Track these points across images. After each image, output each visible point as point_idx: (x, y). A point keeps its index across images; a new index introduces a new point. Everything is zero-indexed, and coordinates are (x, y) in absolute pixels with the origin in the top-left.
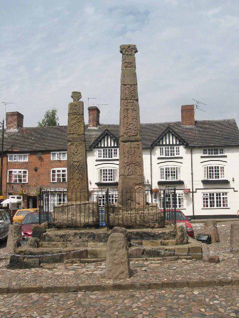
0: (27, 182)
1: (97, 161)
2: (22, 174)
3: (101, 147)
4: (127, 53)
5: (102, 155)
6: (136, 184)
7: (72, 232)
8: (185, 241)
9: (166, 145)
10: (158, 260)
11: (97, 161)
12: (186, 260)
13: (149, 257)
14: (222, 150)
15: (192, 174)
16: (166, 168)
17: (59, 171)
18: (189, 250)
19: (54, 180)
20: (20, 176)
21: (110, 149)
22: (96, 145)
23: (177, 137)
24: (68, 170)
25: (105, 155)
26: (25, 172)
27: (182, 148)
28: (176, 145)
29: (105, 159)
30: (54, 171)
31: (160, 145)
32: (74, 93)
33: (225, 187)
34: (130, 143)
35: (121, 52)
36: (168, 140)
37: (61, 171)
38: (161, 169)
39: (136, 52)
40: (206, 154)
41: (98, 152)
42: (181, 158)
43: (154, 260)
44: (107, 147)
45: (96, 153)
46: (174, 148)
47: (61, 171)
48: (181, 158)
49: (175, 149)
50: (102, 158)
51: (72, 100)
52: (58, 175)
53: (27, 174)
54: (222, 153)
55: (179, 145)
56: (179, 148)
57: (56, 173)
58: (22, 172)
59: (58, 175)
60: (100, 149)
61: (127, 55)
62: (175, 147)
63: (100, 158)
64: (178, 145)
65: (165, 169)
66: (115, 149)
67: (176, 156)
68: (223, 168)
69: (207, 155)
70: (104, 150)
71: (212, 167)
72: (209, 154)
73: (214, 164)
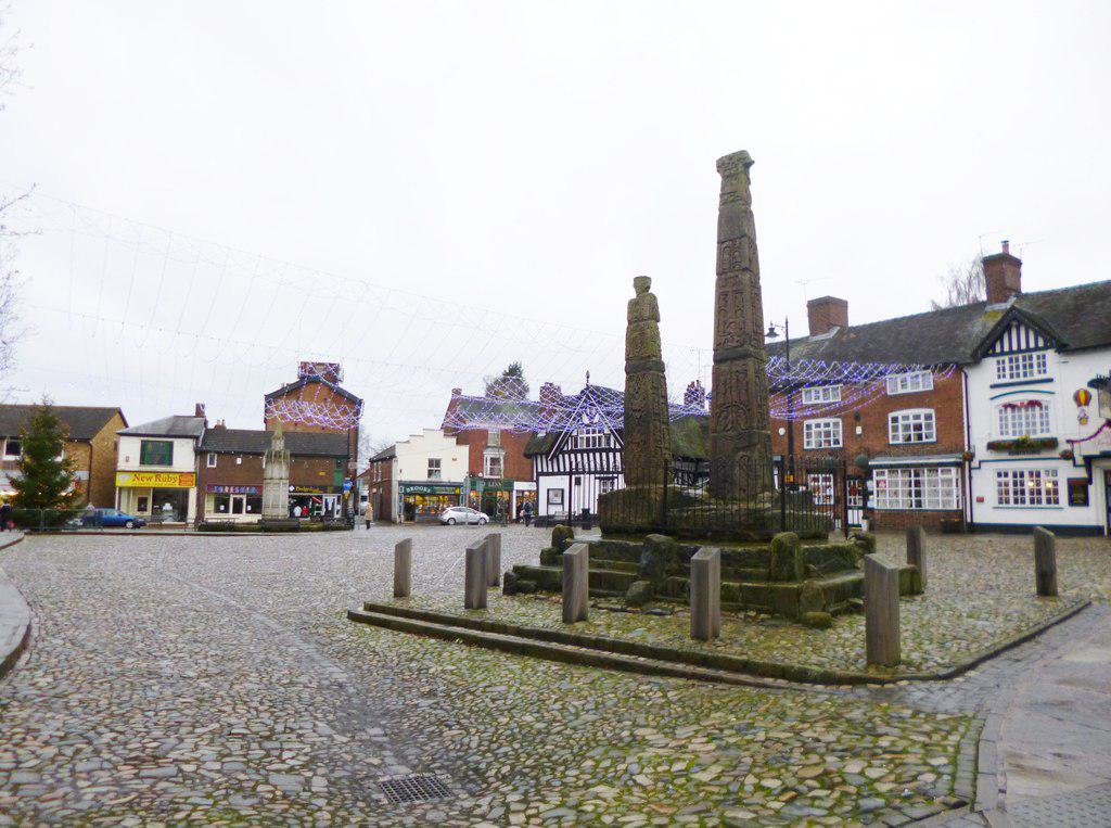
0: (841, 445)
1: (993, 387)
2: (922, 421)
3: (1003, 353)
5: (1008, 372)
6: (739, 449)
7: (1075, 609)
9: (1011, 352)
11: (993, 387)
17: (818, 426)
19: (808, 443)
20: (918, 427)
21: (1027, 354)
22: (986, 348)
23: (1041, 331)
24: (937, 412)
25: (1015, 372)
26: (836, 424)
27: (1051, 355)
28: (1037, 348)
29: (1016, 380)
30: (809, 427)
31: (995, 355)
32: (636, 279)
33: (1049, 456)
34: (728, 363)
36: (550, 466)
37: (911, 417)
41: (995, 367)
42: (1051, 380)
44: (594, 451)
45: (990, 364)
46: (1031, 358)
47: (911, 417)
48: (1051, 380)
49: (1035, 361)
50: (1007, 380)
52: (907, 427)
53: (934, 421)
55: (1046, 348)
56: (1044, 357)
57: (901, 422)
58: (923, 418)
59: (907, 427)
60: (1001, 358)
62: (1035, 355)
63: (1002, 381)
64: (1040, 349)
66: (1041, 353)
67: (1037, 377)
70: (1011, 360)
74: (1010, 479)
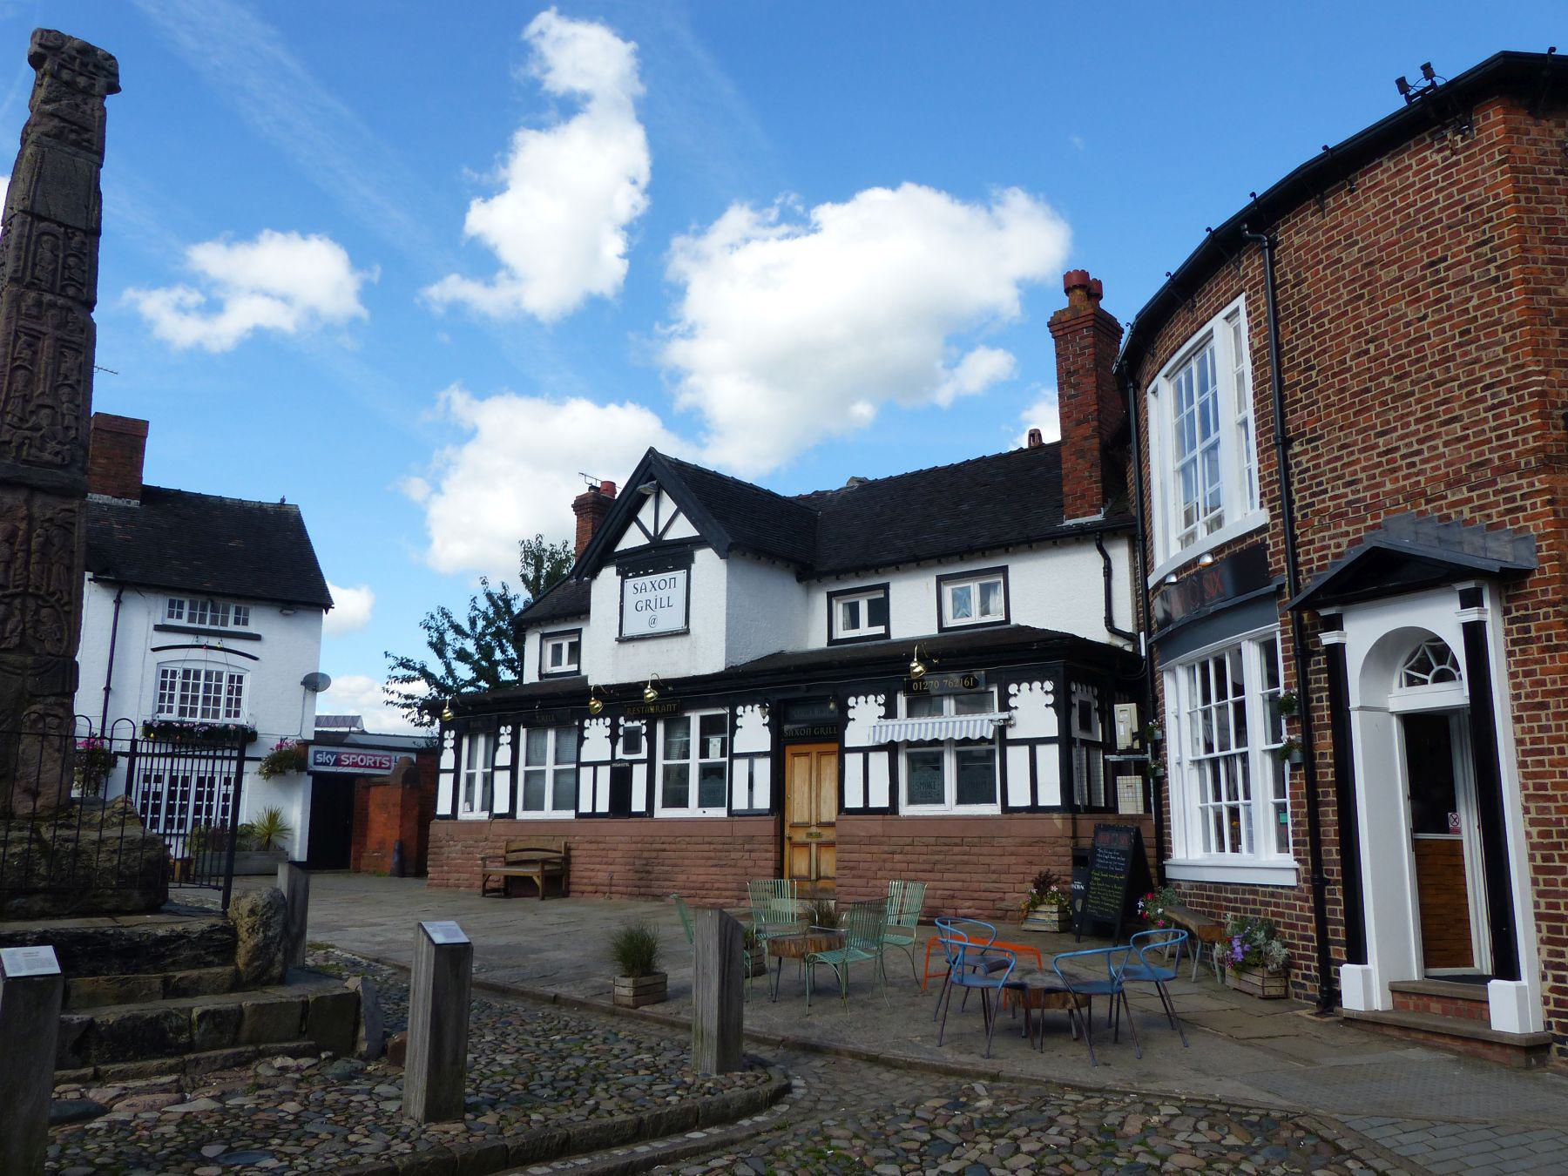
4: (66, 75)
8: (276, 971)
10: (161, 1072)
12: (290, 1062)
13: (114, 1060)
14: (247, 614)
15: (108, 689)
16: (186, 673)
18: (303, 1017)
35: (36, 61)
38: (165, 673)
39: (114, 88)
40: (180, 616)
43: (139, 1075)
51: (1063, 302)
54: (245, 623)
61: (67, 84)
65: (180, 673)
68: (240, 679)
69: (183, 622)
71: (197, 675)
72: (214, 622)
73: (199, 660)
74: (164, 787)
